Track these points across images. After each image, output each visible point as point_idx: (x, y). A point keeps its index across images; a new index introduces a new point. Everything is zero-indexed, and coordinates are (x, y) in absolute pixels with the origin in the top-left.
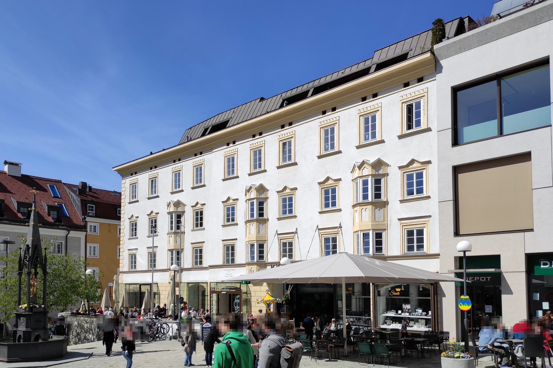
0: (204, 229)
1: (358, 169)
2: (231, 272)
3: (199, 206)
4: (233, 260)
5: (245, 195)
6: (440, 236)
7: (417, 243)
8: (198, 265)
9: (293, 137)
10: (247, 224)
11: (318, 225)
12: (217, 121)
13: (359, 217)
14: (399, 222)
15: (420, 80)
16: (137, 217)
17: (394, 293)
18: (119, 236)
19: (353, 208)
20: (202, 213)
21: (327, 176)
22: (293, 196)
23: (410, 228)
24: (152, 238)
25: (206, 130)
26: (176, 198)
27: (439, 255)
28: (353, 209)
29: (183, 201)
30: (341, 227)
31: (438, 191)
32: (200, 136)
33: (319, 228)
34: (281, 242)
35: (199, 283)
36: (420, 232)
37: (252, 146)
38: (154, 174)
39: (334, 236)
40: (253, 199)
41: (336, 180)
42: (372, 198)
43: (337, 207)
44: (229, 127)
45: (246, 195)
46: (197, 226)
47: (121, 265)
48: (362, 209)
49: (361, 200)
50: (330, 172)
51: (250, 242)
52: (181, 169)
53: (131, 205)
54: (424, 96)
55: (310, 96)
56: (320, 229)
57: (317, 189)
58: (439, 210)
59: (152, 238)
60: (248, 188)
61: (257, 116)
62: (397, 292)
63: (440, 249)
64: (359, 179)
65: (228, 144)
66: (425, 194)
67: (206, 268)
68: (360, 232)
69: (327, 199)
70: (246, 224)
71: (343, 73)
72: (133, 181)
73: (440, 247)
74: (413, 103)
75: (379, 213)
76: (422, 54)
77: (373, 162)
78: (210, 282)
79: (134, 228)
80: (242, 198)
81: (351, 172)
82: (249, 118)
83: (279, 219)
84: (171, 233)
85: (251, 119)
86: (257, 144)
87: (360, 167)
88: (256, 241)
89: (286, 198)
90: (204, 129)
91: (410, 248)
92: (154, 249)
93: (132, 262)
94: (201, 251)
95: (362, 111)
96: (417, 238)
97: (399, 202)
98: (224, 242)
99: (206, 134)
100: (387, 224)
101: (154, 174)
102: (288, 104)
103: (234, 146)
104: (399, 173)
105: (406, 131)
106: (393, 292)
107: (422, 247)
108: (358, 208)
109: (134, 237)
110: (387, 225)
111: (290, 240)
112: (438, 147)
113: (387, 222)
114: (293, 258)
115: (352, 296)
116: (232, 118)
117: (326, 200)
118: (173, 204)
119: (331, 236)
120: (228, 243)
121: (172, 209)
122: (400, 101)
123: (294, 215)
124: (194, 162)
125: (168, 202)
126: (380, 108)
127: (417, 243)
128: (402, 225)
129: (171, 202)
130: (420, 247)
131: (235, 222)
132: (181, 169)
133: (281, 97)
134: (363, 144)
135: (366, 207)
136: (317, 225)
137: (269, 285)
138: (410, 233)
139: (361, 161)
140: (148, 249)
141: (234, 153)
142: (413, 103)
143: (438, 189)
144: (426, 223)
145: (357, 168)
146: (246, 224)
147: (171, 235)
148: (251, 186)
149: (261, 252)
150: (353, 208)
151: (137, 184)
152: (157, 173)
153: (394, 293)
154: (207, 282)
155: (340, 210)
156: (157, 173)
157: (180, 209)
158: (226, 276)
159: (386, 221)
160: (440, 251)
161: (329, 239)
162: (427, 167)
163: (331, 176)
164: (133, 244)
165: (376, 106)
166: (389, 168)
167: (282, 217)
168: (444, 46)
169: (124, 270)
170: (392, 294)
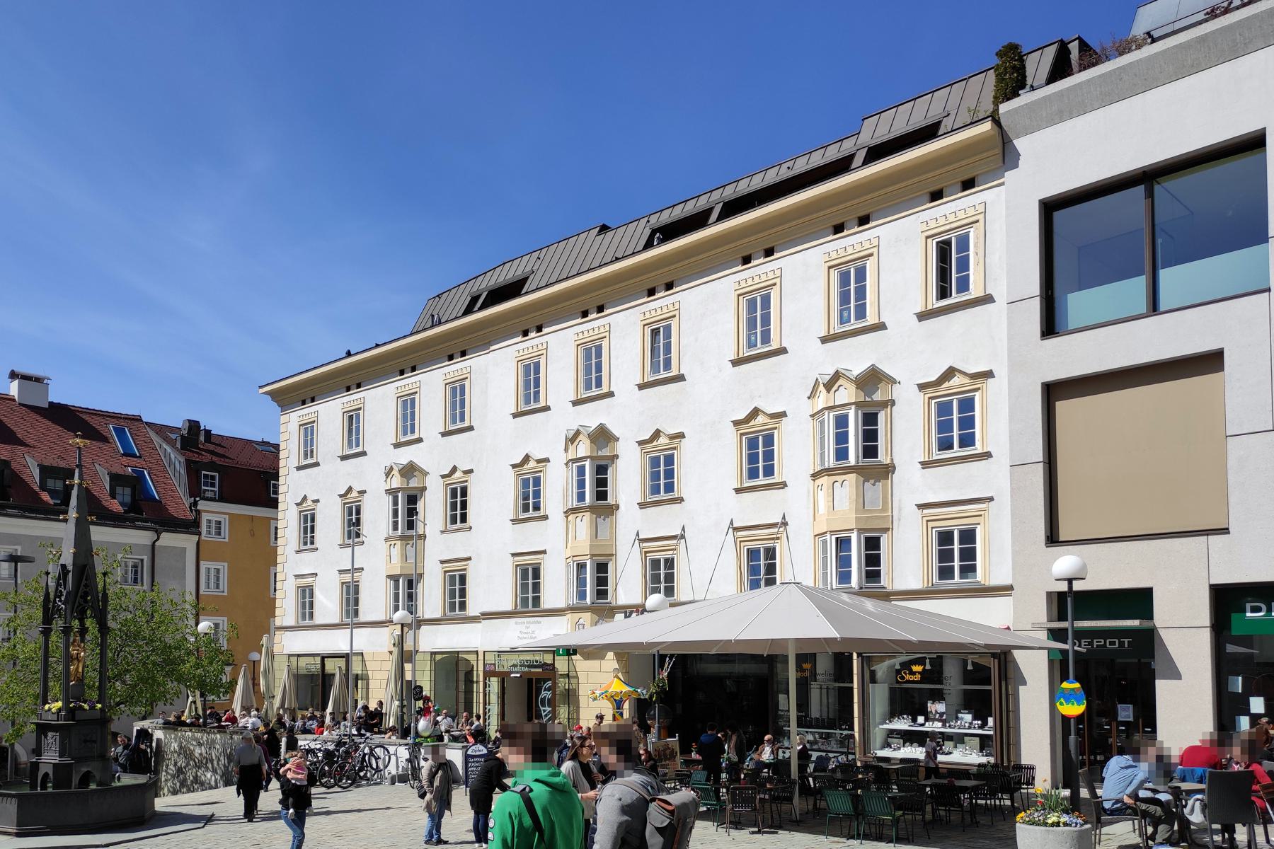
0: (471, 528)
1: (824, 391)
2: (533, 627)
3: (458, 476)
4: (537, 600)
5: (565, 450)
6: (1013, 543)
7: (960, 562)
8: (457, 612)
9: (674, 316)
10: (570, 518)
11: (732, 520)
12: (501, 279)
13: (828, 502)
14: (919, 513)
16: (316, 501)
17: (908, 677)
18: (274, 545)
19: (814, 480)
20: (464, 492)
21: (753, 407)
22: (675, 451)
23: (945, 525)
24: (350, 549)
25: (474, 299)
26: (405, 456)
27: (1011, 588)
28: (812, 482)
29: (421, 463)
30: (785, 524)
31: (1010, 440)
32: (460, 314)
33: (735, 526)
34: (648, 558)
35: (458, 652)
36: (968, 536)
37: (581, 336)
38: (355, 401)
39: (769, 544)
40: (584, 459)
41: (773, 416)
42: (857, 457)
43: (776, 478)
44: (527, 293)
45: (566, 450)
46: (454, 521)
47: (278, 612)
48: (834, 482)
49: (831, 461)
50: (760, 396)
51: (575, 559)
52: (418, 389)
53: (302, 472)
54: (977, 221)
55: (715, 222)
56: (737, 529)
57: (731, 435)
58: (1011, 484)
59: (350, 549)
60: (572, 433)
61: (591, 267)
62: (914, 673)
63: (1014, 575)
64: (826, 413)
65: (525, 333)
66: (979, 448)
67: (474, 619)
68: (828, 535)
69: (753, 459)
70: (567, 517)
71: (791, 168)
72: (307, 417)
73: (1013, 569)
74: (951, 238)
75: (874, 491)
76: (971, 123)
77: (860, 374)
78: (484, 652)
79: (308, 525)
80: (559, 458)
81: (809, 398)
82: (574, 272)
83: (643, 505)
84: (395, 537)
85: (578, 274)
86: (591, 333)
88: (589, 557)
89: (659, 457)
90: (469, 298)
91: (945, 573)
92: (355, 574)
93: (304, 604)
94: (463, 579)
95: (834, 255)
96: (961, 550)
97: (920, 466)
98: (516, 558)
99: (475, 310)
100: (890, 517)
101: (355, 401)
102: (663, 241)
103: (540, 336)
104: (920, 398)
105: (934, 303)
106: (905, 673)
107: (973, 569)
108: (824, 480)
109: (309, 546)
110: (890, 519)
111: (668, 554)
112: (1010, 338)
113: (892, 513)
114: (675, 595)
115: (812, 683)
116: (533, 272)
117: (750, 462)
118: (399, 471)
119: (762, 545)
120: (525, 560)
121: (396, 482)
122: (922, 232)
123: (676, 496)
124: (448, 375)
125: (388, 465)
126: (876, 249)
127: (960, 562)
128: (925, 519)
130: (968, 570)
131: (542, 513)
132: (418, 389)
133: (648, 224)
134: (836, 332)
135: (843, 477)
136: (730, 520)
137: (619, 657)
138: (945, 538)
139: (832, 372)
140: (342, 576)
141: (540, 353)
142: (951, 238)
143: (1010, 437)
144: (981, 515)
145: (821, 388)
146: (567, 517)
147: (393, 543)
148: (578, 430)
149: (602, 582)
150: (814, 480)
151: (315, 424)
152: (362, 399)
153: (908, 677)
154: (477, 651)
155: (783, 485)
156: (362, 399)
157: (414, 483)
158: (521, 636)
159: (890, 510)
160: (1014, 578)
161: (758, 551)
162: (984, 385)
163: (762, 406)
164: (306, 563)
165: (867, 245)
166: (896, 387)
167: (650, 500)
168: (1022, 106)
169: (286, 624)
170: (903, 678)
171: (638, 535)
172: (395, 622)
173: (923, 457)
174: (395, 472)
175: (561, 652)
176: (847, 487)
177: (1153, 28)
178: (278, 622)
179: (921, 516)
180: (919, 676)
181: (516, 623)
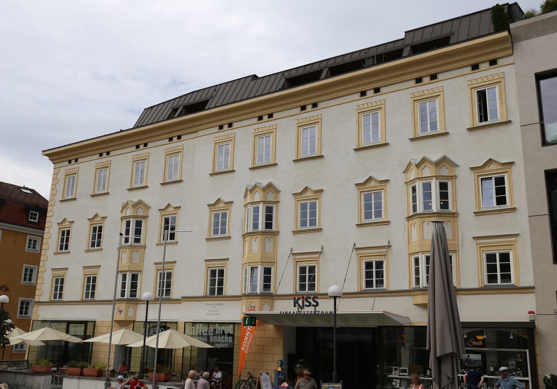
0: (102, 249)
1: (249, 194)
2: (217, 308)
3: (171, 210)
4: (220, 291)
5: (244, 197)
6: (533, 262)
7: (376, 278)
8: (89, 298)
9: (146, 159)
10: (246, 239)
11: (355, 243)
12: (197, 99)
13: (420, 234)
14: (474, 242)
15: (493, 62)
16: (104, 218)
17: (474, 343)
18: (31, 250)
19: (408, 221)
20: (100, 229)
21: (489, 158)
22: (318, 201)
23: (491, 251)
24: (163, 247)
25: (175, 110)
26: (135, 197)
27: (533, 288)
28: (407, 222)
29: (145, 200)
30: (389, 246)
31: (528, 202)
32: (165, 119)
33: (294, 252)
34: (298, 265)
35: (166, 322)
36: (505, 257)
37: (257, 131)
38: (72, 170)
39: (379, 259)
40: (259, 202)
41: (316, 192)
42: (437, 208)
43: (383, 219)
44: (209, 109)
45: (245, 197)
46: (61, 248)
47: (37, 292)
48: (423, 222)
49: (251, 229)
50: (373, 170)
51: (250, 264)
52: (109, 165)
53: (64, 204)
54: (440, 95)
55: (324, 78)
56: (294, 254)
57: (354, 193)
58: (530, 227)
59: (163, 247)
60: (251, 187)
61: (217, 105)
62: (478, 341)
63: (535, 280)
64: (418, 181)
65: (303, 108)
66: (508, 205)
67: (177, 301)
68: (420, 254)
69: (216, 224)
70: (244, 238)
71: (367, 53)
72: (69, 171)
73: (535, 277)
74: (485, 89)
75: (269, 243)
76: (478, 37)
77: (438, 160)
78: (185, 322)
79: (65, 236)
80: (239, 201)
81: (404, 172)
82: (145, 124)
83: (295, 232)
84: (126, 246)
85: (261, 95)
86: (264, 129)
87: (251, 191)
88: (260, 263)
89: (306, 204)
90: (171, 110)
91: (369, 284)
92: (165, 265)
93: (88, 287)
94: (95, 279)
95: (361, 107)
96: (376, 271)
97: (205, 240)
98: (208, 263)
99: (175, 116)
100: (457, 244)
101: (72, 170)
102: (187, 113)
103: (76, 164)
104: (292, 200)
105: (478, 123)
106: (472, 340)
107: (382, 282)
108: (417, 221)
109: (64, 250)
110: (457, 245)
111: (312, 264)
112: (524, 145)
113: (458, 242)
114: (316, 289)
115: (402, 347)
116: (212, 97)
117: (366, 208)
118: (132, 205)
119: (374, 260)
120: (215, 264)
121: (129, 212)
122: (297, 124)
123: (317, 228)
124: (98, 164)
125: (125, 201)
126: (148, 157)
127: (376, 278)
128: (479, 246)
129: (129, 202)
130: (380, 282)
131: (227, 235)
132: (109, 165)
133: (283, 76)
134: (419, 136)
135: (126, 250)
136: (291, 249)
137: (278, 328)
138: (303, 270)
139: (253, 184)
140: (85, 270)
141: (230, 139)
142: (485, 89)
143: (527, 199)
144: (513, 245)
145: (249, 192)
146: (244, 238)
147: (124, 250)
148: (256, 185)
149: (134, 286)
150: (408, 221)
151: (76, 175)
152: (78, 168)
153: (474, 343)
154: (177, 322)
155: (387, 223)
156: (78, 168)
157: (140, 213)
158: (209, 313)
159: (457, 240)
160: (535, 283)
161: (305, 268)
162: (510, 170)
163: (374, 176)
164: (62, 261)
165: (379, 103)
166: (457, 169)
167: (300, 230)
168: (523, 25)
169: (42, 300)
170: (471, 343)
171: (291, 251)
172: (329, 295)
173: (358, 221)
174: (130, 206)
175: (247, 324)
176: (256, 243)
177: (257, 82)
178: (37, 299)
179: (205, 265)
180: (481, 342)
181: (206, 304)
